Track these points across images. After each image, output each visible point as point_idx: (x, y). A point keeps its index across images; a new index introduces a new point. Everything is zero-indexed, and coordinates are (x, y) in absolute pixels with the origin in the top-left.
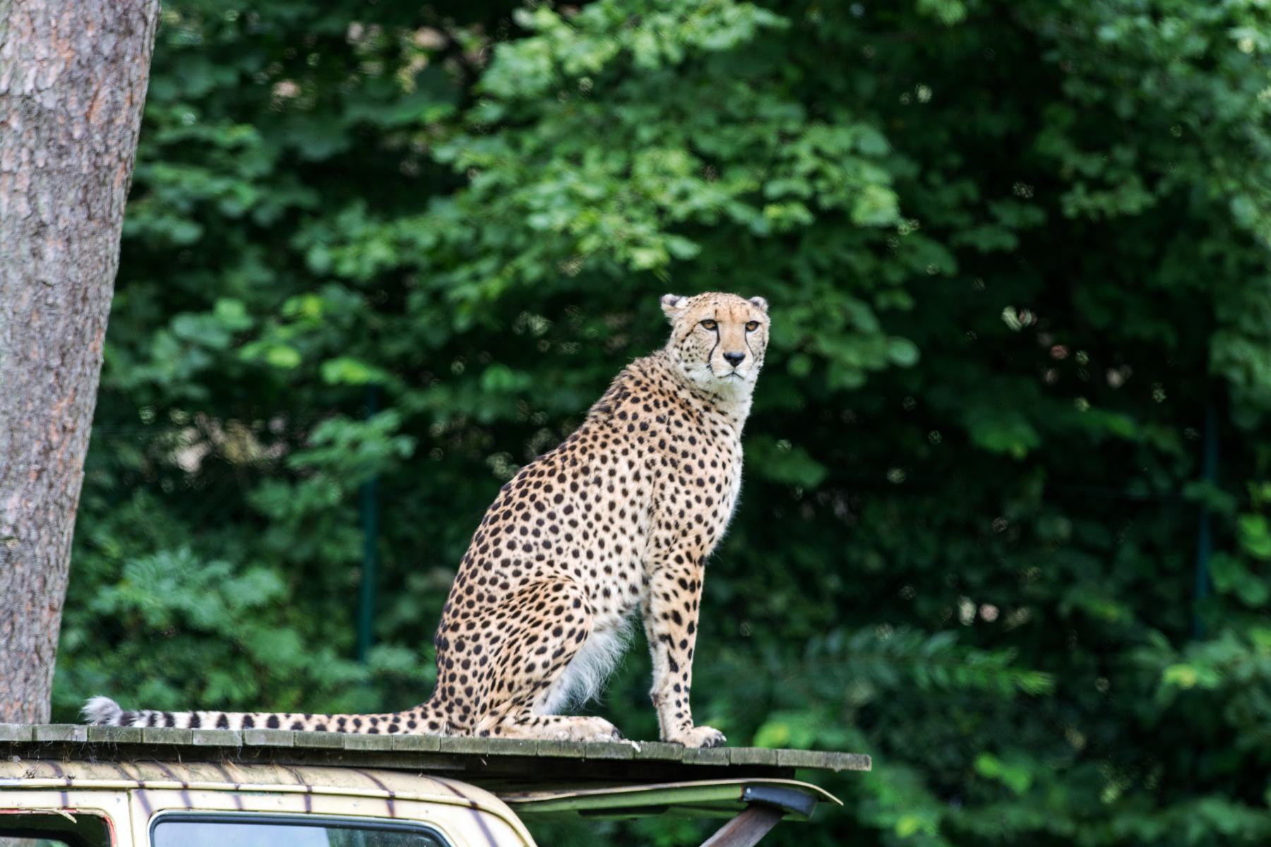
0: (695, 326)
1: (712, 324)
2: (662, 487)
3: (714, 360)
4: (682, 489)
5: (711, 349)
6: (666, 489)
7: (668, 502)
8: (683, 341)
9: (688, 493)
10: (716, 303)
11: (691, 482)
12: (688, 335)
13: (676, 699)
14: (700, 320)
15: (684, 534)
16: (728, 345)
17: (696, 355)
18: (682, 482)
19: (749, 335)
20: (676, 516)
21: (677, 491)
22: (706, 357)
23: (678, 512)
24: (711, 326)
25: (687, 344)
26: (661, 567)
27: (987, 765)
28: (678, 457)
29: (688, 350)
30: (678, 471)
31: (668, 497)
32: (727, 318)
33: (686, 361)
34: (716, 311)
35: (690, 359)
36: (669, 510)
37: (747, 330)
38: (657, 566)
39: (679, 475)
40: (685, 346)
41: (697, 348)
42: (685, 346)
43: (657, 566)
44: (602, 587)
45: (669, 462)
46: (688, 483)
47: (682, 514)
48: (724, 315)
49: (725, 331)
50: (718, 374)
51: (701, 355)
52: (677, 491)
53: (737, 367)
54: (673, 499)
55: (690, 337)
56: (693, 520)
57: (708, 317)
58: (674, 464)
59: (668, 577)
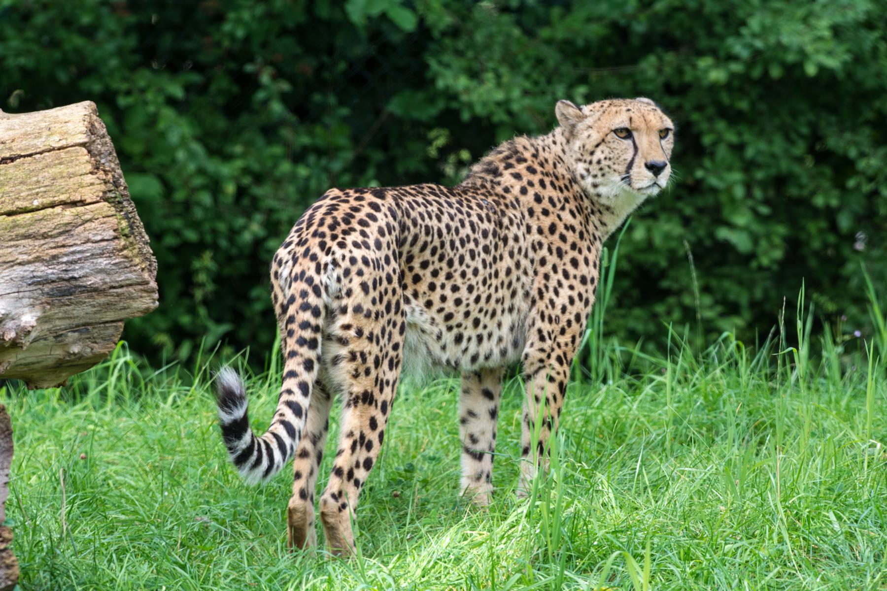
0: (607, 135)
1: (627, 133)
2: (547, 277)
3: (634, 171)
4: (565, 283)
5: (630, 159)
6: (550, 281)
7: (551, 294)
8: (592, 153)
9: (571, 288)
10: (629, 110)
11: (575, 277)
12: (597, 146)
13: (541, 437)
14: (613, 128)
15: (563, 332)
16: (648, 154)
17: (609, 167)
18: (566, 275)
19: (663, 142)
20: (558, 311)
21: (560, 284)
22: (622, 168)
23: (560, 307)
24: (623, 135)
25: (598, 155)
26: (544, 367)
27: (317, 98)
28: (566, 247)
29: (599, 162)
30: (562, 263)
31: (551, 289)
32: (643, 126)
33: (595, 176)
34: (631, 119)
35: (599, 174)
36: (552, 302)
37: (661, 138)
38: (541, 365)
39: (562, 267)
40: (595, 158)
41: (610, 159)
42: (595, 158)
43: (541, 365)
44: (461, 329)
45: (554, 251)
46: (571, 277)
47: (564, 310)
48: (638, 122)
49: (643, 140)
50: (637, 185)
51: (616, 167)
52: (560, 284)
53: (659, 177)
54: (556, 293)
55: (601, 148)
56: (572, 318)
57: (622, 125)
58: (560, 253)
59: (551, 379)
